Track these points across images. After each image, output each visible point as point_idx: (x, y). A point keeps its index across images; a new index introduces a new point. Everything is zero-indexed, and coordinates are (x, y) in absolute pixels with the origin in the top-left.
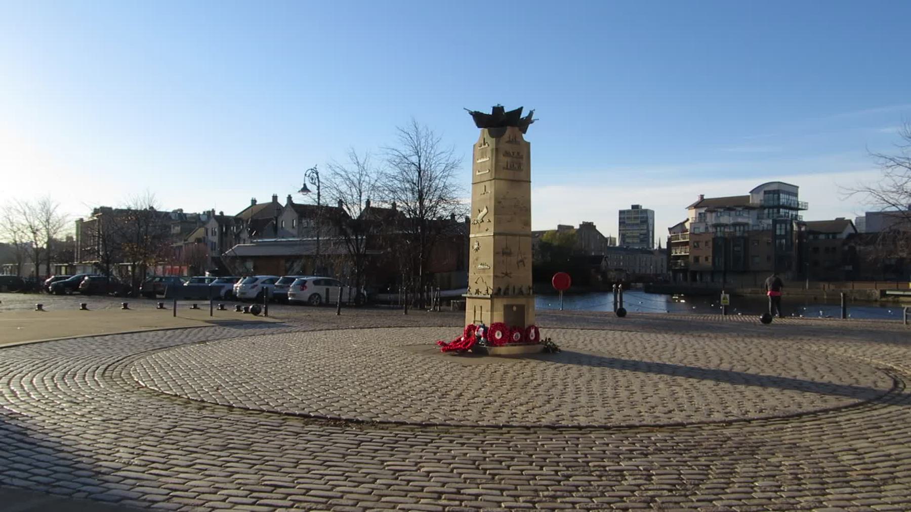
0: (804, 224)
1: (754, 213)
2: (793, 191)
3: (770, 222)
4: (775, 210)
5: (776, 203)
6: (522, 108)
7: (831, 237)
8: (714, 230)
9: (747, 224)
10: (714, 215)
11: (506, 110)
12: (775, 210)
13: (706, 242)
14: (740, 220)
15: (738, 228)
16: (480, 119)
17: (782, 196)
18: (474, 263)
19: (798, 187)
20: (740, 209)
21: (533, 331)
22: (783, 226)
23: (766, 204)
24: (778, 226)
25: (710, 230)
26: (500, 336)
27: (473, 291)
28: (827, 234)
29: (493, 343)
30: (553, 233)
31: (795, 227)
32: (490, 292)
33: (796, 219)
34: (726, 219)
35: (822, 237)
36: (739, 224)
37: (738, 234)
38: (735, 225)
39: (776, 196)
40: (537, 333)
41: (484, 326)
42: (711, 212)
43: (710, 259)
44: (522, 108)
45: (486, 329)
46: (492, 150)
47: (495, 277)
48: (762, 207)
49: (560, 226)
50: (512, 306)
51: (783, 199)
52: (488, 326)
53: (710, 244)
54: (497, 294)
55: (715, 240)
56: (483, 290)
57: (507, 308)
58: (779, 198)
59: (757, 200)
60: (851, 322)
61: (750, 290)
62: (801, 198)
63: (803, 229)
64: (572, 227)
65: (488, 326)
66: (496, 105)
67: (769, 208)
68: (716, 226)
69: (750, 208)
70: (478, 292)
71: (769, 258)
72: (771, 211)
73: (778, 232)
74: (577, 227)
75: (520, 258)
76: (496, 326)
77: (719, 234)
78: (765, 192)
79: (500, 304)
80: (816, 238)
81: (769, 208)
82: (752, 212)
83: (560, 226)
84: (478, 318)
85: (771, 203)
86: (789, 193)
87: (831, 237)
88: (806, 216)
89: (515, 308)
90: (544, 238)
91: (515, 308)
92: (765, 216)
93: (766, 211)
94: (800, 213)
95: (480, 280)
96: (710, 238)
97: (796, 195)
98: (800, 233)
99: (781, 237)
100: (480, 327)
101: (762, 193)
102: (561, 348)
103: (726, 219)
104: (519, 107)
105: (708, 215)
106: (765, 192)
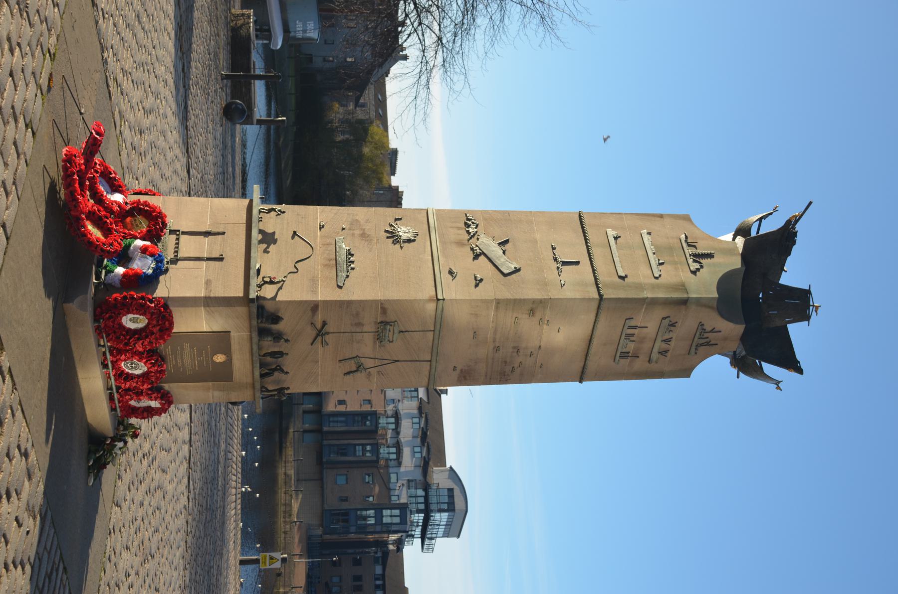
0: (399, 549)
1: (418, 475)
2: (454, 530)
3: (403, 500)
4: (422, 507)
5: (433, 507)
6: (800, 371)
7: (378, 582)
8: (390, 413)
9: (400, 464)
10: (416, 411)
11: (795, 330)
12: (422, 507)
13: (369, 402)
14: (406, 452)
15: (393, 420)
16: (768, 249)
17: (445, 516)
18: (355, 223)
19: (458, 537)
20: (424, 454)
21: (155, 404)
22: (397, 520)
23: (432, 493)
24: (397, 512)
25: (390, 408)
26: (133, 326)
27: (270, 223)
28: (383, 577)
29: (106, 314)
30: (382, 144)
31: (393, 537)
32: (268, 292)
33: (408, 536)
34: (408, 430)
35: (378, 570)
36: (399, 453)
37: (383, 451)
38: (398, 446)
39: (445, 507)
40: (148, 413)
41: (159, 271)
42: (420, 409)
43: (341, 408)
44: (800, 371)
45: (151, 280)
46: (682, 287)
47: (315, 307)
48: (426, 487)
49: (395, 152)
50: (228, 352)
51: (441, 518)
52: (161, 291)
53: (366, 408)
54: (264, 317)
55: (374, 415)
56: (268, 263)
57: (221, 340)
58: (440, 511)
59: (438, 477)
60: (272, 160)
61: (291, 472)
62: (441, 543)
63: (391, 547)
64: (393, 173)
65: (161, 291)
66: (816, 299)
67: (426, 497)
68: (397, 416)
69: (425, 467)
70: (268, 239)
71: (344, 499)
72: (422, 500)
73: (386, 512)
74: (395, 181)
75: (368, 363)
76: (162, 316)
77: (382, 421)
78: (451, 491)
79: (236, 326)
80: (376, 560)
81: (426, 497)
82: (419, 471)
83: (395, 152)
84: (189, 247)
85: (433, 500)
86: (449, 525)
87: (378, 582)
88: (411, 552)
89: (220, 358)
90: (375, 129)
91: (220, 358)
92: (412, 491)
93: (421, 492)
94: (417, 542)
95: (304, 251)
96: (378, 407)
97: (447, 534)
98: (385, 544)
99: (379, 517)
100: (159, 260)
101: (451, 484)
102: (109, 473)
103: (408, 430)
104: (800, 354)
105: (415, 404)
106: (451, 491)
